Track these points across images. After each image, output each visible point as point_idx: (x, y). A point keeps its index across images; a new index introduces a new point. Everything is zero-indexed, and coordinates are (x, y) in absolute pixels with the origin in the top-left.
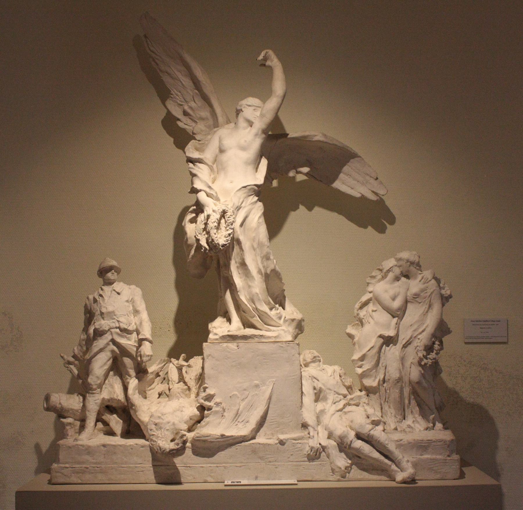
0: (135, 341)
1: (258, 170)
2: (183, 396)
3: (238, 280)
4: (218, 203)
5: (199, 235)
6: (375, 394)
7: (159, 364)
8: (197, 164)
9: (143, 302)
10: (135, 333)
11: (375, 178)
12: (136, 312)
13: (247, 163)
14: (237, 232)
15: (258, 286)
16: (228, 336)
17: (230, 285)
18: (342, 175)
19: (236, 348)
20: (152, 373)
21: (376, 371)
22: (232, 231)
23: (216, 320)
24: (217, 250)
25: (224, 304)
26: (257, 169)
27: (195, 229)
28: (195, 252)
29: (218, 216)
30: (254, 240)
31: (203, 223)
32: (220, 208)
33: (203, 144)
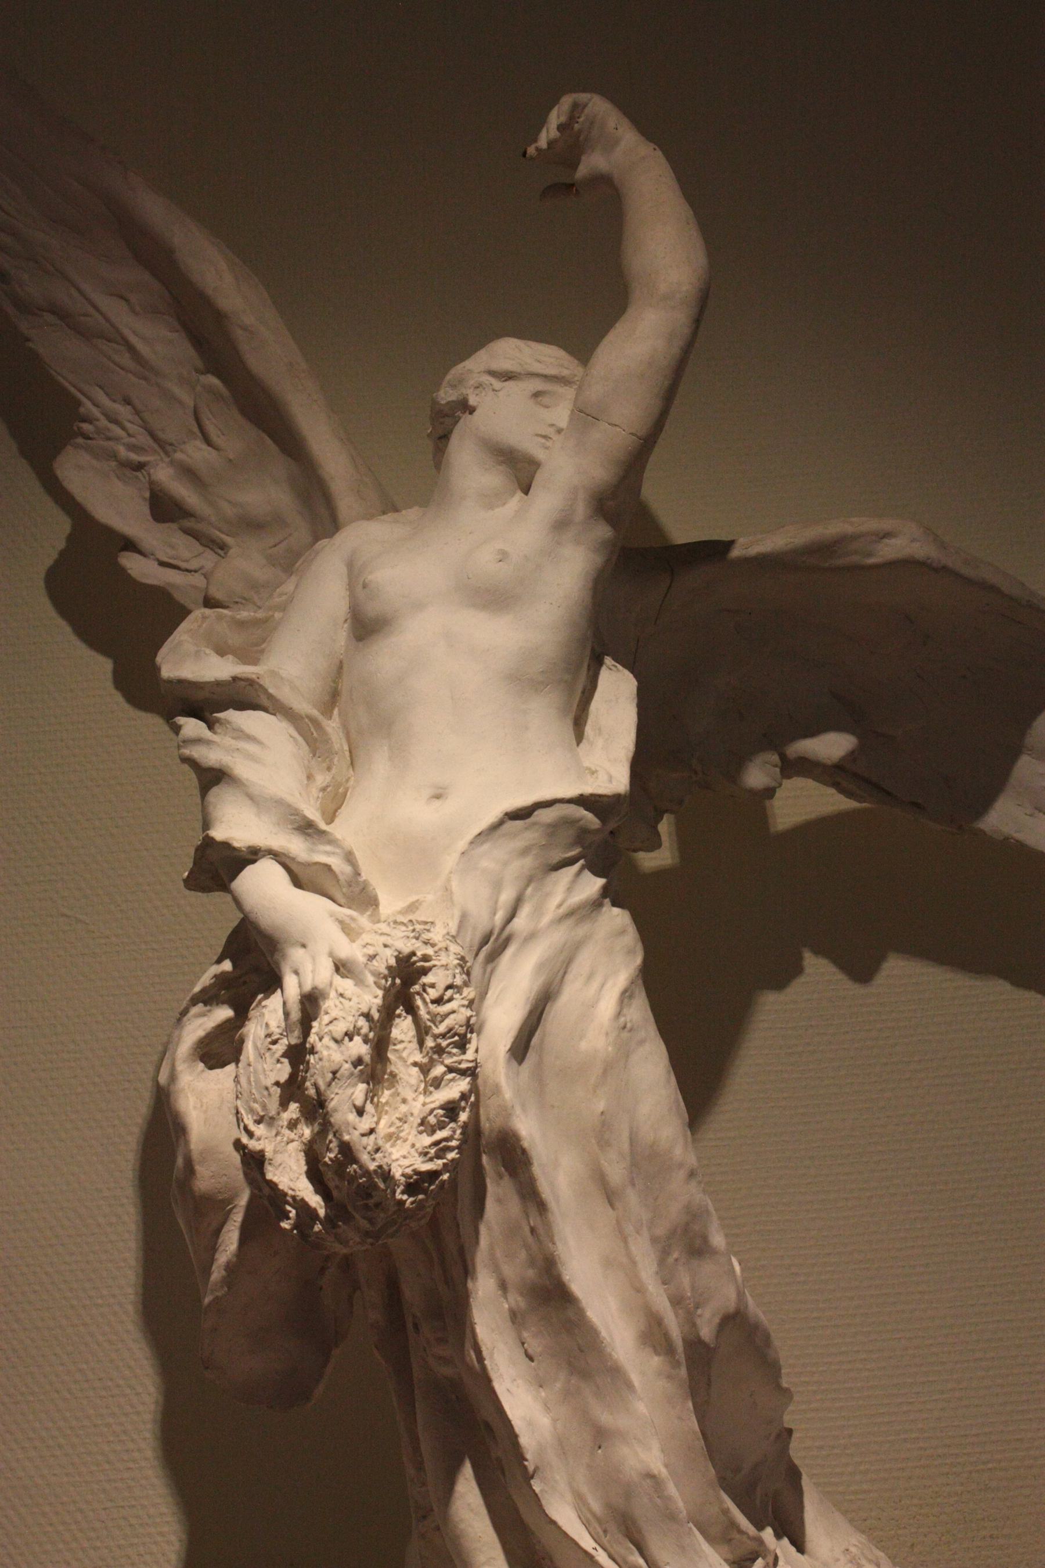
1: (588, 730)
3: (524, 1402)
4: (363, 920)
5: (260, 1130)
8: (232, 715)
14: (497, 1090)
15: (651, 1432)
18: (1026, 767)
22: (464, 1084)
24: (381, 1217)
27: (231, 1096)
28: (243, 1240)
29: (372, 999)
30: (602, 1132)
31: (280, 1048)
32: (380, 942)
33: (256, 623)
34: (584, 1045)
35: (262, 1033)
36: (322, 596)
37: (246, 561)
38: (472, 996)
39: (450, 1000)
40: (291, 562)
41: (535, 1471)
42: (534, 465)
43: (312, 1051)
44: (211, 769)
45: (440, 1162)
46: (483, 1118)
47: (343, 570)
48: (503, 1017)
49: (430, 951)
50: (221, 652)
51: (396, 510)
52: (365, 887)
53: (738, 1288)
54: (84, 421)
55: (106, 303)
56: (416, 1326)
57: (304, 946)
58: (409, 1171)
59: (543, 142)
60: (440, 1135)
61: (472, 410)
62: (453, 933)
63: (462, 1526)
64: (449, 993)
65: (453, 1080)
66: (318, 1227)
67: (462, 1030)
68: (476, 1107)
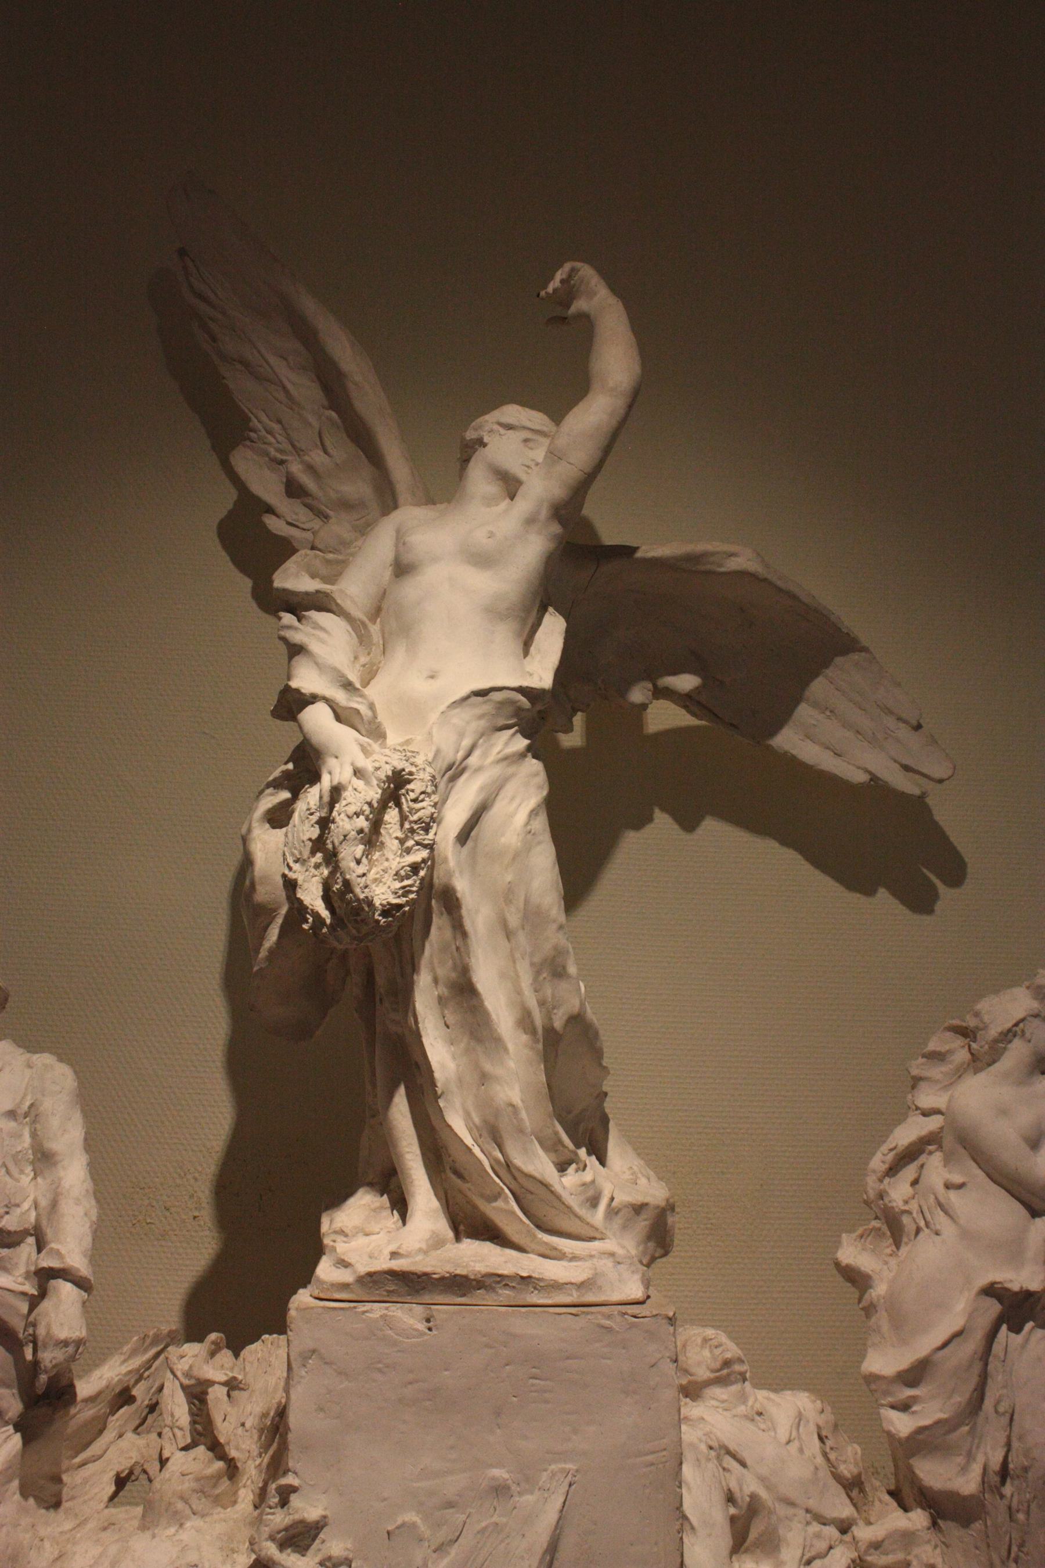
0: (27, 1276)
1: (532, 649)
2: (198, 1504)
3: (441, 1053)
4: (376, 746)
5: (296, 867)
6: (966, 1522)
7: (134, 1353)
8: (313, 614)
9: (77, 1117)
10: (31, 1240)
11: (914, 723)
12: (44, 1159)
13: (493, 612)
14: (445, 860)
15: (516, 1077)
16: (392, 1273)
17: (411, 1069)
18: (804, 711)
19: (422, 1326)
20: (91, 1400)
21: (972, 1432)
22: (425, 853)
23: (351, 1201)
24: (365, 929)
25: (386, 1143)
26: (527, 645)
27: (281, 846)
29: (374, 794)
30: (508, 895)
31: (315, 818)
32: (384, 760)
33: (338, 562)
34: (503, 840)
35: (305, 807)
36: (380, 547)
37: (339, 527)
38: (436, 800)
39: (423, 801)
40: (364, 529)
41: (443, 1093)
42: (519, 483)
43: (333, 822)
44: (295, 645)
45: (405, 899)
46: (435, 876)
47: (394, 534)
48: (455, 816)
49: (414, 769)
50: (313, 576)
51: (434, 504)
52: (379, 726)
53: (581, 1001)
54: (251, 431)
55: (273, 360)
56: (381, 1000)
57: (337, 757)
58: (384, 902)
59: (550, 289)
60: (406, 882)
61: (485, 445)
62: (430, 760)
63: (395, 1123)
64: (422, 796)
65: (418, 850)
66: (325, 930)
67: (428, 820)
68: (431, 869)
